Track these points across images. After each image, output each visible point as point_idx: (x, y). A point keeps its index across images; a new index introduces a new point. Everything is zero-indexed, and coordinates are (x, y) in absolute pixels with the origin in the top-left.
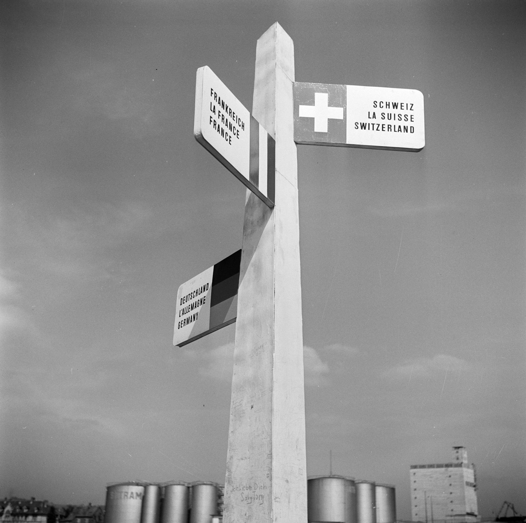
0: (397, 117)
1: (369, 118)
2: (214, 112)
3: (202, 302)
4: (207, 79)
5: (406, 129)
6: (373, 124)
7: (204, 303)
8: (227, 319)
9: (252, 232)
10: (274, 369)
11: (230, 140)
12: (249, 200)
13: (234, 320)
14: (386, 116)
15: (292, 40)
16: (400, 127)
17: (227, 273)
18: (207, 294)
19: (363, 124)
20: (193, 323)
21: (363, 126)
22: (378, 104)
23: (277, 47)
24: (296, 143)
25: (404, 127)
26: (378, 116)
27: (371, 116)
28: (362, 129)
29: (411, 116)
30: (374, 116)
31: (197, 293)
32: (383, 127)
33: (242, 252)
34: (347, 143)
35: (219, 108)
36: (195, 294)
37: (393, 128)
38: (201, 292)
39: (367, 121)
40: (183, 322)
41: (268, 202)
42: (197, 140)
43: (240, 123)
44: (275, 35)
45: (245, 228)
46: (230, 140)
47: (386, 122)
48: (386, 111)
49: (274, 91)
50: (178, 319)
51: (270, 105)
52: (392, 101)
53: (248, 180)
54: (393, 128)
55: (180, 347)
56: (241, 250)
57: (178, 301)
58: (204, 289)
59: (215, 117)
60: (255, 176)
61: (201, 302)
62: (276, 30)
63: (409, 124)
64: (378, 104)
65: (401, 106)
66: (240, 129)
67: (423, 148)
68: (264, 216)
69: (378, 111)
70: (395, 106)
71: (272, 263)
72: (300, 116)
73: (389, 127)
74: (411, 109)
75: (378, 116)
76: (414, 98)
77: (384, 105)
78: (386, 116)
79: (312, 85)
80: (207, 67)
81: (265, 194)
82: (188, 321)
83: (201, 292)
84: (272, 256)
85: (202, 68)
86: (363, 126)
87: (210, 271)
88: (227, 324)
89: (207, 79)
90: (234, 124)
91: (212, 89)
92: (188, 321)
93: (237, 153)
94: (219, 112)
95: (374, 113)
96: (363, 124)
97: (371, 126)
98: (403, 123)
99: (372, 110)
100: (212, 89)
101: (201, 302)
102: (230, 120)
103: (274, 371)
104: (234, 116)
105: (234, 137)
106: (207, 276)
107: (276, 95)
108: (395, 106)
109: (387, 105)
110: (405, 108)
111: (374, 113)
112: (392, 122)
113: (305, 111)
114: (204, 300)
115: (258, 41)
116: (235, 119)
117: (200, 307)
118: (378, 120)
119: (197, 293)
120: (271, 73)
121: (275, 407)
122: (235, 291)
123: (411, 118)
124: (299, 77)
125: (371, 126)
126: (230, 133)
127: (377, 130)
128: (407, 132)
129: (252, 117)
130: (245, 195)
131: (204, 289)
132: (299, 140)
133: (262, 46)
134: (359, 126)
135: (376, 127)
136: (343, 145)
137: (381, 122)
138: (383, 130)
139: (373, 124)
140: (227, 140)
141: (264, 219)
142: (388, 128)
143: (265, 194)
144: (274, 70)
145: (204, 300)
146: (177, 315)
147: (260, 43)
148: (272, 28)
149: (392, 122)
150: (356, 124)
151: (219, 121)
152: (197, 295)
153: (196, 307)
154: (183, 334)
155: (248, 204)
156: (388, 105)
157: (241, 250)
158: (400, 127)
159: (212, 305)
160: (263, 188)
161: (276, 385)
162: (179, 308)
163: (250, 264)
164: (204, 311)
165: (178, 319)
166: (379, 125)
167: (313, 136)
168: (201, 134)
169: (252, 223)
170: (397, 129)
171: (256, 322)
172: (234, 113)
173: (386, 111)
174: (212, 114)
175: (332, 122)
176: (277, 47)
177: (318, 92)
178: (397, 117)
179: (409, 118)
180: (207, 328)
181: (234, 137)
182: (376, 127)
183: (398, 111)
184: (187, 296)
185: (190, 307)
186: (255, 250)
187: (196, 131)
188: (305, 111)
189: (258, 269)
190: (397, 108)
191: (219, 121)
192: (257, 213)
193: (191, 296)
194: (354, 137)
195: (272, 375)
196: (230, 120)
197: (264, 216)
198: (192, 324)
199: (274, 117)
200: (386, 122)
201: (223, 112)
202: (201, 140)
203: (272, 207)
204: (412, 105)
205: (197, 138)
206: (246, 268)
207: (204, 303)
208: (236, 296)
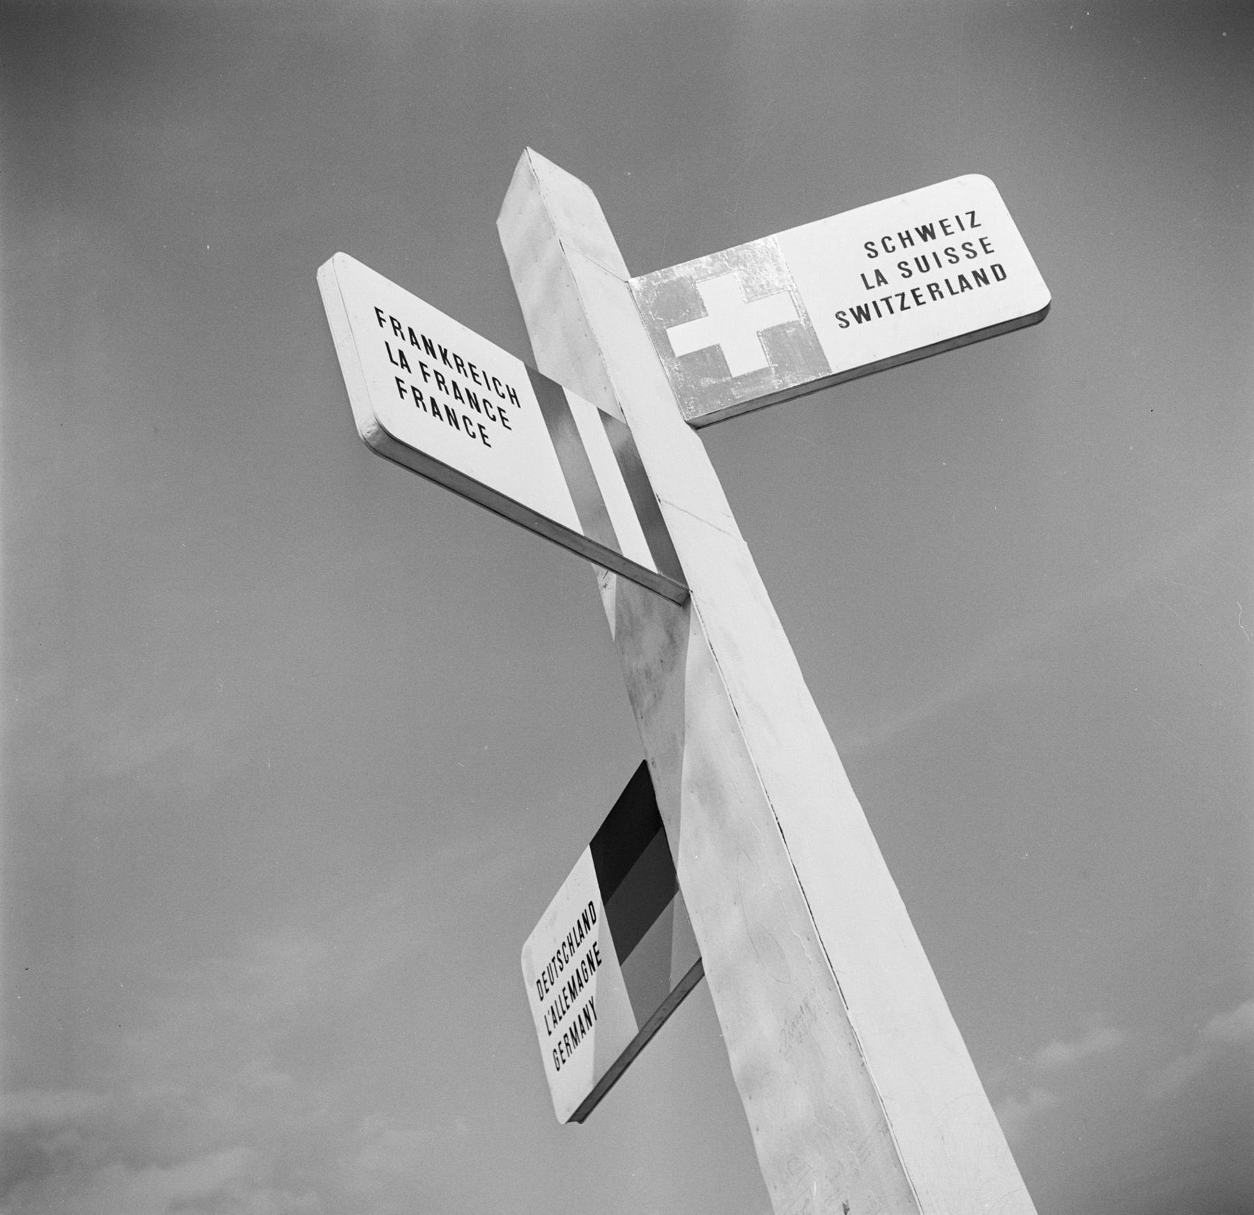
0: (944, 259)
1: (868, 288)
2: (405, 365)
3: (592, 962)
4: (351, 289)
5: (981, 277)
6: (886, 300)
7: (599, 963)
8: (676, 976)
9: (658, 697)
10: (866, 1059)
11: (483, 436)
12: (619, 616)
13: (697, 972)
14: (913, 266)
15: (586, 187)
16: (961, 278)
17: (633, 849)
18: (600, 932)
19: (859, 308)
20: (591, 1032)
21: (861, 314)
22: (879, 247)
23: (553, 211)
24: (696, 427)
25: (975, 273)
26: (892, 273)
27: (872, 280)
28: (860, 322)
29: (981, 240)
30: (880, 278)
31: (571, 944)
32: (916, 297)
33: (651, 768)
34: (835, 372)
35: (415, 355)
36: (567, 949)
37: (944, 288)
38: (582, 936)
39: (864, 298)
40: (563, 1046)
41: (669, 588)
42: (376, 451)
43: (503, 390)
44: (533, 178)
45: (633, 699)
46: (483, 436)
47: (920, 280)
48: (908, 254)
49: (581, 308)
50: (547, 1044)
51: (584, 346)
52: (912, 224)
53: (580, 531)
54: (944, 288)
55: (581, 1121)
56: (645, 762)
57: (532, 991)
58: (586, 922)
59: (413, 378)
60: (593, 507)
61: (591, 963)
62: (534, 165)
63: (983, 262)
64: (879, 247)
65: (944, 228)
66: (506, 403)
67: (1047, 309)
68: (671, 637)
69: (887, 263)
70: (927, 233)
71: (743, 752)
72: (678, 354)
73: (933, 289)
74: (973, 225)
75: (892, 273)
76: (973, 196)
77: (896, 241)
78: (913, 266)
79: (681, 271)
80: (340, 257)
81: (649, 563)
82: (574, 1036)
83: (582, 936)
84: (735, 730)
85: (329, 262)
86: (861, 314)
87: (585, 867)
88: (683, 992)
89: (351, 289)
90: (481, 392)
91: (377, 310)
92: (574, 1036)
93: (515, 458)
94: (422, 365)
95: (878, 272)
96: (859, 308)
97: (883, 306)
98: (966, 267)
99: (869, 267)
100: (377, 310)
101: (591, 963)
102: (465, 383)
103: (868, 1066)
104: (474, 374)
105: (493, 429)
106: (582, 883)
107: (588, 316)
108: (927, 233)
109: (903, 240)
110: (955, 227)
111: (878, 272)
112: (935, 275)
113: (686, 339)
114: (597, 954)
115: (499, 222)
116: (481, 379)
117: (593, 978)
118: (897, 284)
119: (571, 944)
120: (559, 274)
121: (918, 1179)
122: (671, 886)
123: (984, 246)
124: (638, 263)
125: (883, 306)
126: (477, 417)
127: (903, 308)
128: (987, 282)
129: (533, 373)
130: (603, 609)
131: (586, 922)
132: (700, 413)
133: (512, 228)
134: (850, 317)
135: (895, 303)
136: (826, 383)
137: (906, 286)
138: (918, 304)
139: (886, 300)
140: (474, 436)
141: (675, 643)
142: (932, 293)
143: (649, 563)
144: (563, 260)
145: (597, 954)
146: (542, 1032)
147: (503, 224)
148: (521, 171)
149: (935, 275)
150: (839, 315)
151: (429, 389)
152: (573, 951)
153: (581, 985)
154: (571, 1082)
155: (619, 632)
156: (906, 239)
157: (645, 762)
158: (961, 278)
159: (622, 959)
160: (635, 546)
161: (893, 1111)
162: (540, 1010)
163: (683, 785)
164: (610, 986)
165: (547, 1044)
166: (903, 295)
167: (733, 390)
168: (382, 428)
169: (648, 674)
170: (956, 286)
171: (761, 942)
172: (471, 365)
173: (908, 254)
174: (402, 373)
175: (774, 338)
176: (553, 211)
177: (704, 278)
178: (944, 259)
179: (977, 247)
180: (630, 1029)
181: (493, 429)
182: (895, 303)
183: (940, 243)
184: (549, 968)
185: (567, 992)
186: (683, 743)
187: (365, 427)
188: (686, 339)
189: (710, 789)
190: (933, 237)
191: (429, 389)
192: (652, 637)
193: (559, 960)
194: (848, 350)
195: (869, 1079)
196: (465, 383)
197: (672, 641)
198: (588, 1040)
199: (604, 371)
200: (920, 280)
201: (434, 364)
202: (390, 448)
203: (684, 600)
204: (973, 213)
205: (373, 443)
206: (676, 803)
207: (599, 963)
208: (677, 896)
